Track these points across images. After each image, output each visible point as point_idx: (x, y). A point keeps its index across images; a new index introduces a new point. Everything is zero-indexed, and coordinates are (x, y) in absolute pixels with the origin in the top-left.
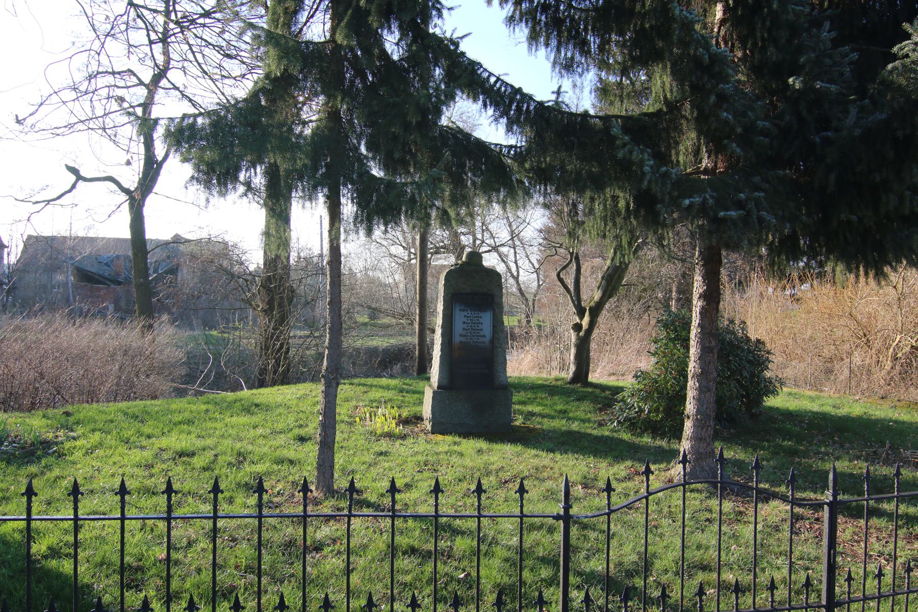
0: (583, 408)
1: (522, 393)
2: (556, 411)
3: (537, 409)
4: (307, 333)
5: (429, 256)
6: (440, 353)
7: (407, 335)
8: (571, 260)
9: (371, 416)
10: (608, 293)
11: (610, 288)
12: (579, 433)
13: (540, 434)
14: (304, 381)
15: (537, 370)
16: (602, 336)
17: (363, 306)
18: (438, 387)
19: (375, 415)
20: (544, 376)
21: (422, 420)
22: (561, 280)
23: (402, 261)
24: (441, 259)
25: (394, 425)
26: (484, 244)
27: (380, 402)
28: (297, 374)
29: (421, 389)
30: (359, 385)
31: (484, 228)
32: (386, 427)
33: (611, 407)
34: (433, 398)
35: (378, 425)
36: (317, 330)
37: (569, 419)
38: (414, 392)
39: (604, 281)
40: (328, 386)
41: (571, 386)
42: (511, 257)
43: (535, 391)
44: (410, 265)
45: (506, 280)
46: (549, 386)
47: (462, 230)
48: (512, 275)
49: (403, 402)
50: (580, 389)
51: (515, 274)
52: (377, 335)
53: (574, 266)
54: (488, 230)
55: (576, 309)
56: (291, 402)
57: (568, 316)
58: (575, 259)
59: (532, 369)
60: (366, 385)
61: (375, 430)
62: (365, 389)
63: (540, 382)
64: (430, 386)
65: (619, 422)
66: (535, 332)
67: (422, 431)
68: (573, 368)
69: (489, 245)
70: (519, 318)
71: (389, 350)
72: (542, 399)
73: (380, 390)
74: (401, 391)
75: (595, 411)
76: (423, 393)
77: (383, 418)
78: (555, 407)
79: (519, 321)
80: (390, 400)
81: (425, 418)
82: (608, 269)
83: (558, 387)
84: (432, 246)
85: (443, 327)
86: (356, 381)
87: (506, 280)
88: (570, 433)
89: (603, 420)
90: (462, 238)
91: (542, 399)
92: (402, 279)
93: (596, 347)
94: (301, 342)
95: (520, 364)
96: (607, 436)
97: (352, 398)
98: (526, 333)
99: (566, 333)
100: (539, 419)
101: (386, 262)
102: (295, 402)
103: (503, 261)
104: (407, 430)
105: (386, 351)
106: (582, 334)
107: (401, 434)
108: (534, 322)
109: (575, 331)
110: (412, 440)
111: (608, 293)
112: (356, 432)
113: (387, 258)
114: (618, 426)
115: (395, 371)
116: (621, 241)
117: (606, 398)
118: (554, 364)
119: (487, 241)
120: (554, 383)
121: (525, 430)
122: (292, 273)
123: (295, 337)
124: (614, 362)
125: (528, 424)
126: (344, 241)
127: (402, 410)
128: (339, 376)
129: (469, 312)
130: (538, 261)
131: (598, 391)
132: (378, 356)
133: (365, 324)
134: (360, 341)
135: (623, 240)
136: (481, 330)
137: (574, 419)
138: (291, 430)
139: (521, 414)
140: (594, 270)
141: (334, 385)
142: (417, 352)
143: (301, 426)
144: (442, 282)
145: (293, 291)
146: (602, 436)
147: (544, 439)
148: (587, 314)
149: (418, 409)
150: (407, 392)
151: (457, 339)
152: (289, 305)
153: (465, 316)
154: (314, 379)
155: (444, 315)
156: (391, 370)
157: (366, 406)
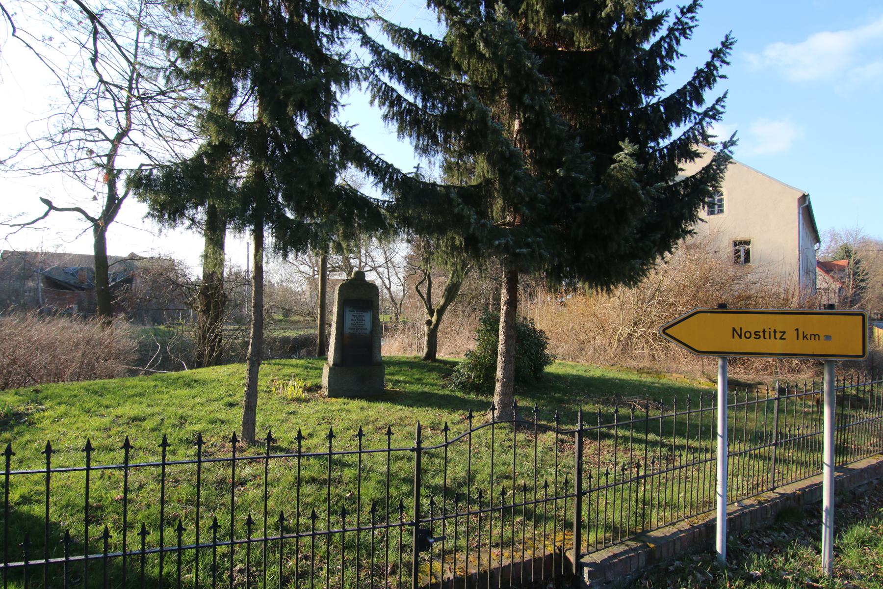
1: (392, 368)
3: (402, 378)
4: (237, 327)
9: (283, 386)
14: (233, 362)
15: (402, 351)
16: (445, 328)
18: (333, 365)
20: (407, 355)
22: (419, 291)
25: (301, 392)
27: (291, 376)
29: (321, 367)
30: (275, 364)
34: (329, 372)
37: (423, 384)
38: (316, 369)
44: (314, 279)
48: (386, 287)
51: (388, 286)
52: (289, 328)
62: (280, 367)
65: (455, 385)
66: (401, 326)
68: (426, 350)
74: (306, 368)
75: (440, 378)
76: (322, 369)
79: (391, 318)
80: (298, 375)
85: (337, 323)
86: (273, 361)
90: (352, 261)
91: (405, 371)
92: (308, 289)
95: (391, 347)
100: (402, 385)
101: (297, 277)
104: (310, 396)
105: (296, 340)
106: (432, 327)
110: (313, 403)
117: (447, 369)
118: (414, 347)
123: (226, 330)
125: (396, 388)
131: (442, 365)
133: (281, 321)
137: (427, 384)
140: (440, 284)
141: (257, 365)
143: (230, 395)
146: (444, 395)
148: (435, 314)
149: (318, 380)
151: (347, 331)
154: (241, 360)
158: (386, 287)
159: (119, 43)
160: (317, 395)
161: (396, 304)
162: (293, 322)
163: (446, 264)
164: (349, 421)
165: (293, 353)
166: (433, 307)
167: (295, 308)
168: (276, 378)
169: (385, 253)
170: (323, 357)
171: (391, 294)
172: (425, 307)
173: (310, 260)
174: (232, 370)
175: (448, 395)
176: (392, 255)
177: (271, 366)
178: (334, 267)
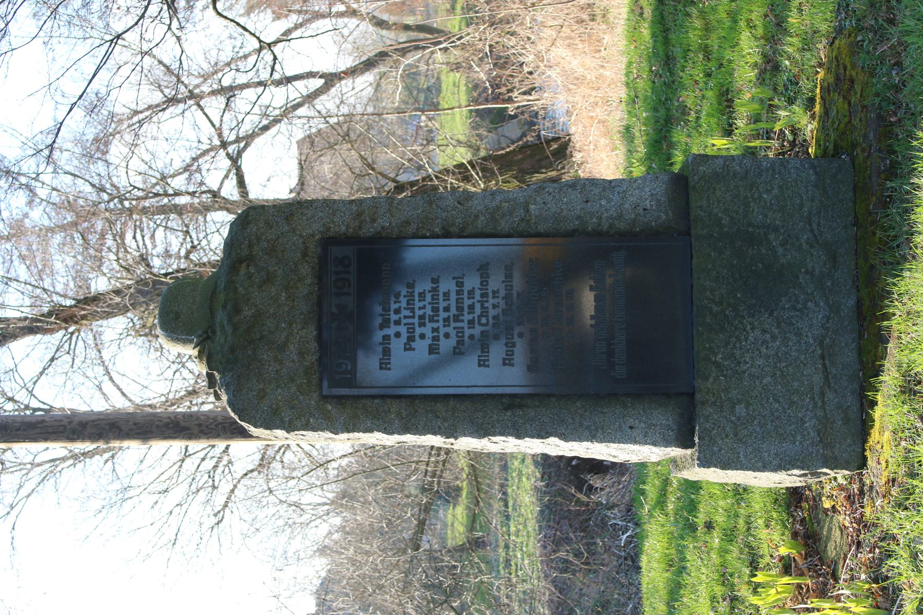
13: (856, 48)
15: (599, 27)
18: (686, 443)
43: (678, 51)
59: (597, 46)
79: (457, 67)
91: (707, 29)
95: (579, 80)
100: (791, 46)
121: (840, 104)
130: (277, 17)
149: (758, 504)
153: (408, 348)
155: (405, 430)
164: (832, 5)
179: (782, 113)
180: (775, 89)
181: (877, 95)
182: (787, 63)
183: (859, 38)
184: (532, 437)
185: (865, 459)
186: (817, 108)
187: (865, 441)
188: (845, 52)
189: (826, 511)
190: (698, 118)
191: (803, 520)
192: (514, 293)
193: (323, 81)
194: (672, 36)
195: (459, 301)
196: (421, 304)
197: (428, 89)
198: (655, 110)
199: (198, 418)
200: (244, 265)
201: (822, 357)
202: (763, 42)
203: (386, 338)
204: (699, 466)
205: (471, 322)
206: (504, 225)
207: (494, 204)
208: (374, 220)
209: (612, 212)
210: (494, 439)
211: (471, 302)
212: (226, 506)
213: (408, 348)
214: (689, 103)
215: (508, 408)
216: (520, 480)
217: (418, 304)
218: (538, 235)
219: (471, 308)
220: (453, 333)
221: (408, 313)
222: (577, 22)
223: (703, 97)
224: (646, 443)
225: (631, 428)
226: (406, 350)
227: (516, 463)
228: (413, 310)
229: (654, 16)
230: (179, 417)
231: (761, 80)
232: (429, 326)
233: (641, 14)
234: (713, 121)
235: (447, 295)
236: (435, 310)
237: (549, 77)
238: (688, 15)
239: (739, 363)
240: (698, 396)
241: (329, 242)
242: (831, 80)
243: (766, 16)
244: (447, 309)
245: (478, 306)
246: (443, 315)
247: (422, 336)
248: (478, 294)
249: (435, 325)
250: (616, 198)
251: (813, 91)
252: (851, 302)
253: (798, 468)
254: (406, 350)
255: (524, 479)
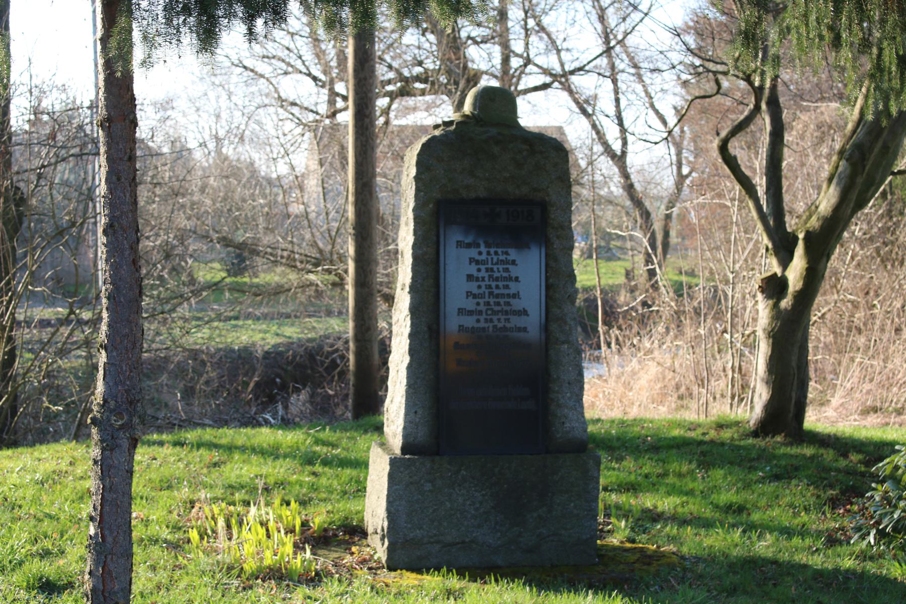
0: (787, 499)
1: (629, 463)
2: (717, 507)
3: (666, 503)
4: (62, 311)
5: (382, 102)
6: (407, 359)
7: (329, 313)
8: (757, 108)
9: (229, 526)
10: (854, 196)
11: (860, 180)
12: (775, 562)
13: (672, 567)
14: (56, 438)
15: (672, 399)
16: (846, 309)
17: (206, 237)
18: (405, 449)
19: (240, 523)
20: (690, 415)
21: (364, 534)
22: (731, 162)
23: (311, 117)
24: (415, 109)
25: (289, 549)
26: (530, 68)
27: (253, 490)
28: (36, 417)
29: (359, 455)
30: (199, 445)
31: (531, 23)
32: (268, 554)
33: (862, 496)
34: (391, 476)
35: (249, 549)
36: (85, 303)
37: (750, 527)
38: (344, 463)
39: (843, 163)
40: (109, 446)
41: (760, 442)
42: (606, 104)
43: (663, 455)
44: (335, 127)
45: (591, 163)
46: (701, 443)
47: (467, 29)
48: (608, 150)
49: (314, 488)
50: (783, 450)
51: (617, 147)
52: (248, 316)
53: (765, 121)
54: (543, 29)
55: (771, 237)
56: (20, 493)
57: (754, 256)
58: (768, 104)
59: (661, 398)
60: (216, 446)
61: (240, 561)
62: (216, 456)
63: (676, 433)
64: (383, 445)
65: (881, 534)
66: (666, 301)
67: (364, 562)
68: (761, 394)
69: (546, 72)
70: (628, 265)
71: (280, 354)
72: (680, 475)
73: (254, 458)
74: (309, 460)
75: (819, 507)
76: (366, 465)
77: (262, 531)
78: (714, 497)
79: (629, 274)
80: (281, 484)
81: (370, 530)
82: (854, 132)
83: (723, 444)
84: (391, 75)
85: (413, 289)
86: (191, 435)
87: (591, 163)
88: (753, 564)
89: (842, 529)
90: (472, 51)
91: (680, 475)
92: (314, 165)
93: (831, 338)
94: (45, 337)
95: (628, 386)
96: (847, 571)
97: (180, 481)
98: (644, 304)
99: (750, 304)
100: (671, 529)
101: (270, 118)
102: (30, 493)
103: (584, 112)
104: (324, 561)
105: (273, 357)
106: (786, 303)
107: (307, 571)
108: (665, 277)
109: (768, 297)
110: (335, 587)
111: (854, 196)
112: (191, 567)
113: (272, 110)
114: (877, 542)
115: (293, 410)
116: (879, 56)
117: (850, 472)
118: (720, 385)
119: (539, 60)
120: (713, 434)
121: (632, 558)
122: (17, 151)
123: (28, 323)
124: (877, 378)
125: (644, 542)
126: (143, 63)
127: (311, 510)
128: (136, 420)
129: (483, 249)
131: (828, 455)
132: (254, 370)
133: (215, 287)
134: (206, 332)
135: (886, 52)
136: (516, 296)
137: (763, 528)
138: (21, 563)
139: (626, 517)
140: (824, 130)
141: (125, 444)
142: (351, 357)
143: (45, 554)
144: (410, 170)
145: (21, 201)
146: (837, 571)
147: (682, 580)
148: (799, 251)
149: (352, 506)
150: (326, 463)
151: (453, 323)
152: (11, 239)
153: (472, 260)
154: (80, 435)
155: (415, 257)
156: (286, 408)
157: (215, 500)
158: (608, 150)
159: (540, 64)
160: (348, 559)
161: (646, 215)
162: (258, 292)
163: (837, 43)
165: (264, 407)
166: (790, 223)
167: (267, 239)
168: (202, 494)
169: (602, 18)
170: (373, 419)
171: (626, 175)
172: (760, 226)
173: (319, 55)
174: (50, 466)
175: (849, 574)
176: (629, 24)
177: (183, 452)
178: (406, 80)
179: (623, 523)
180: (639, 519)
181: (641, 578)
182: (659, 527)
183: (678, 569)
184: (410, 345)
185: (395, 570)
186: (628, 545)
187: (407, 570)
188: (669, 560)
189: (350, 549)
190: (614, 469)
191: (336, 535)
192: (508, 333)
193: (619, 153)
194: (674, 451)
195: (503, 296)
196: (501, 269)
197: (610, 249)
198: (618, 439)
199: (371, 77)
200: (528, 147)
201: (463, 542)
202: (673, 512)
203: (478, 246)
204: (391, 459)
205: (488, 304)
206: (553, 327)
207: (568, 320)
208: (558, 237)
209: (562, 401)
210: (409, 318)
211: (502, 303)
212: (245, 67)
213: (472, 260)
214: (625, 463)
215: (430, 328)
216: (260, 331)
217: (501, 267)
218: (547, 350)
219: (498, 304)
220: (481, 291)
221: (495, 260)
222: (677, 385)
223: (630, 473)
224: (405, 422)
225: (416, 412)
226: (470, 259)
227: (275, 328)
228: (497, 264)
229: (689, 438)
230: (372, 63)
231: (645, 511)
232: (486, 275)
233: (690, 429)
234: (614, 480)
235: (507, 287)
236: (497, 279)
237: (631, 360)
238: (690, 462)
239: (460, 486)
240: (437, 458)
241: (544, 206)
242: (649, 553)
243: (691, 514)
244: (497, 287)
245: (499, 308)
246: (493, 284)
247: (479, 270)
248: (508, 308)
249: (486, 279)
250: (571, 403)
251: (640, 542)
252: (500, 562)
253: (389, 525)
254: (470, 259)
255: (261, 335)
